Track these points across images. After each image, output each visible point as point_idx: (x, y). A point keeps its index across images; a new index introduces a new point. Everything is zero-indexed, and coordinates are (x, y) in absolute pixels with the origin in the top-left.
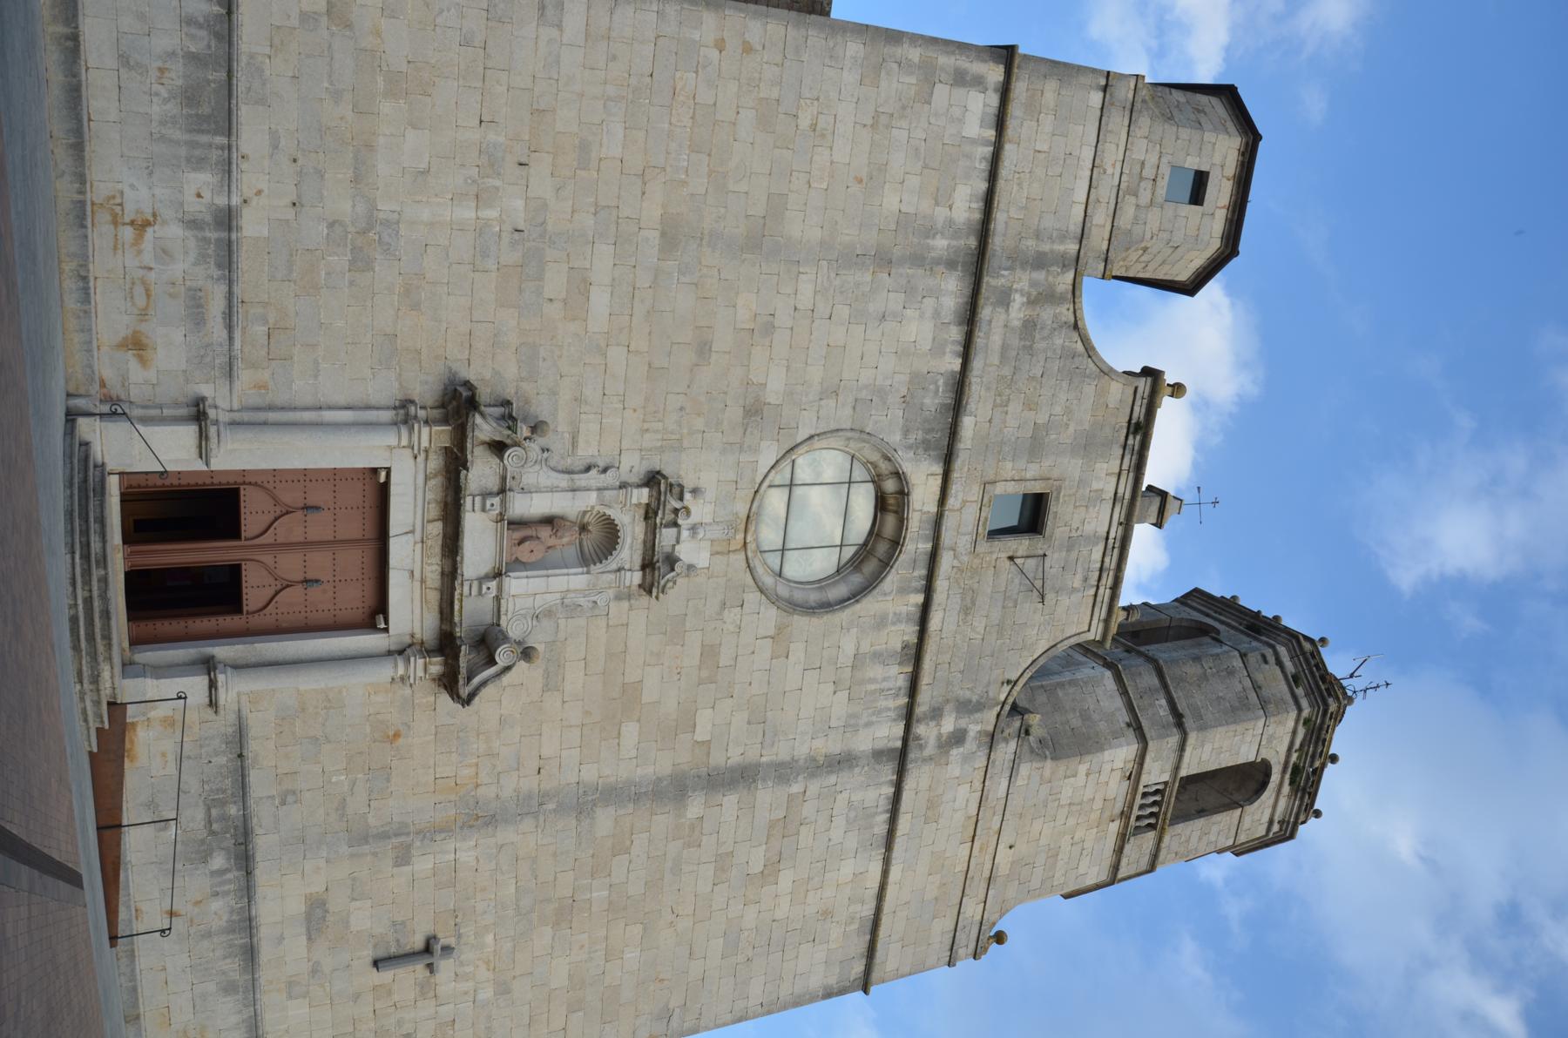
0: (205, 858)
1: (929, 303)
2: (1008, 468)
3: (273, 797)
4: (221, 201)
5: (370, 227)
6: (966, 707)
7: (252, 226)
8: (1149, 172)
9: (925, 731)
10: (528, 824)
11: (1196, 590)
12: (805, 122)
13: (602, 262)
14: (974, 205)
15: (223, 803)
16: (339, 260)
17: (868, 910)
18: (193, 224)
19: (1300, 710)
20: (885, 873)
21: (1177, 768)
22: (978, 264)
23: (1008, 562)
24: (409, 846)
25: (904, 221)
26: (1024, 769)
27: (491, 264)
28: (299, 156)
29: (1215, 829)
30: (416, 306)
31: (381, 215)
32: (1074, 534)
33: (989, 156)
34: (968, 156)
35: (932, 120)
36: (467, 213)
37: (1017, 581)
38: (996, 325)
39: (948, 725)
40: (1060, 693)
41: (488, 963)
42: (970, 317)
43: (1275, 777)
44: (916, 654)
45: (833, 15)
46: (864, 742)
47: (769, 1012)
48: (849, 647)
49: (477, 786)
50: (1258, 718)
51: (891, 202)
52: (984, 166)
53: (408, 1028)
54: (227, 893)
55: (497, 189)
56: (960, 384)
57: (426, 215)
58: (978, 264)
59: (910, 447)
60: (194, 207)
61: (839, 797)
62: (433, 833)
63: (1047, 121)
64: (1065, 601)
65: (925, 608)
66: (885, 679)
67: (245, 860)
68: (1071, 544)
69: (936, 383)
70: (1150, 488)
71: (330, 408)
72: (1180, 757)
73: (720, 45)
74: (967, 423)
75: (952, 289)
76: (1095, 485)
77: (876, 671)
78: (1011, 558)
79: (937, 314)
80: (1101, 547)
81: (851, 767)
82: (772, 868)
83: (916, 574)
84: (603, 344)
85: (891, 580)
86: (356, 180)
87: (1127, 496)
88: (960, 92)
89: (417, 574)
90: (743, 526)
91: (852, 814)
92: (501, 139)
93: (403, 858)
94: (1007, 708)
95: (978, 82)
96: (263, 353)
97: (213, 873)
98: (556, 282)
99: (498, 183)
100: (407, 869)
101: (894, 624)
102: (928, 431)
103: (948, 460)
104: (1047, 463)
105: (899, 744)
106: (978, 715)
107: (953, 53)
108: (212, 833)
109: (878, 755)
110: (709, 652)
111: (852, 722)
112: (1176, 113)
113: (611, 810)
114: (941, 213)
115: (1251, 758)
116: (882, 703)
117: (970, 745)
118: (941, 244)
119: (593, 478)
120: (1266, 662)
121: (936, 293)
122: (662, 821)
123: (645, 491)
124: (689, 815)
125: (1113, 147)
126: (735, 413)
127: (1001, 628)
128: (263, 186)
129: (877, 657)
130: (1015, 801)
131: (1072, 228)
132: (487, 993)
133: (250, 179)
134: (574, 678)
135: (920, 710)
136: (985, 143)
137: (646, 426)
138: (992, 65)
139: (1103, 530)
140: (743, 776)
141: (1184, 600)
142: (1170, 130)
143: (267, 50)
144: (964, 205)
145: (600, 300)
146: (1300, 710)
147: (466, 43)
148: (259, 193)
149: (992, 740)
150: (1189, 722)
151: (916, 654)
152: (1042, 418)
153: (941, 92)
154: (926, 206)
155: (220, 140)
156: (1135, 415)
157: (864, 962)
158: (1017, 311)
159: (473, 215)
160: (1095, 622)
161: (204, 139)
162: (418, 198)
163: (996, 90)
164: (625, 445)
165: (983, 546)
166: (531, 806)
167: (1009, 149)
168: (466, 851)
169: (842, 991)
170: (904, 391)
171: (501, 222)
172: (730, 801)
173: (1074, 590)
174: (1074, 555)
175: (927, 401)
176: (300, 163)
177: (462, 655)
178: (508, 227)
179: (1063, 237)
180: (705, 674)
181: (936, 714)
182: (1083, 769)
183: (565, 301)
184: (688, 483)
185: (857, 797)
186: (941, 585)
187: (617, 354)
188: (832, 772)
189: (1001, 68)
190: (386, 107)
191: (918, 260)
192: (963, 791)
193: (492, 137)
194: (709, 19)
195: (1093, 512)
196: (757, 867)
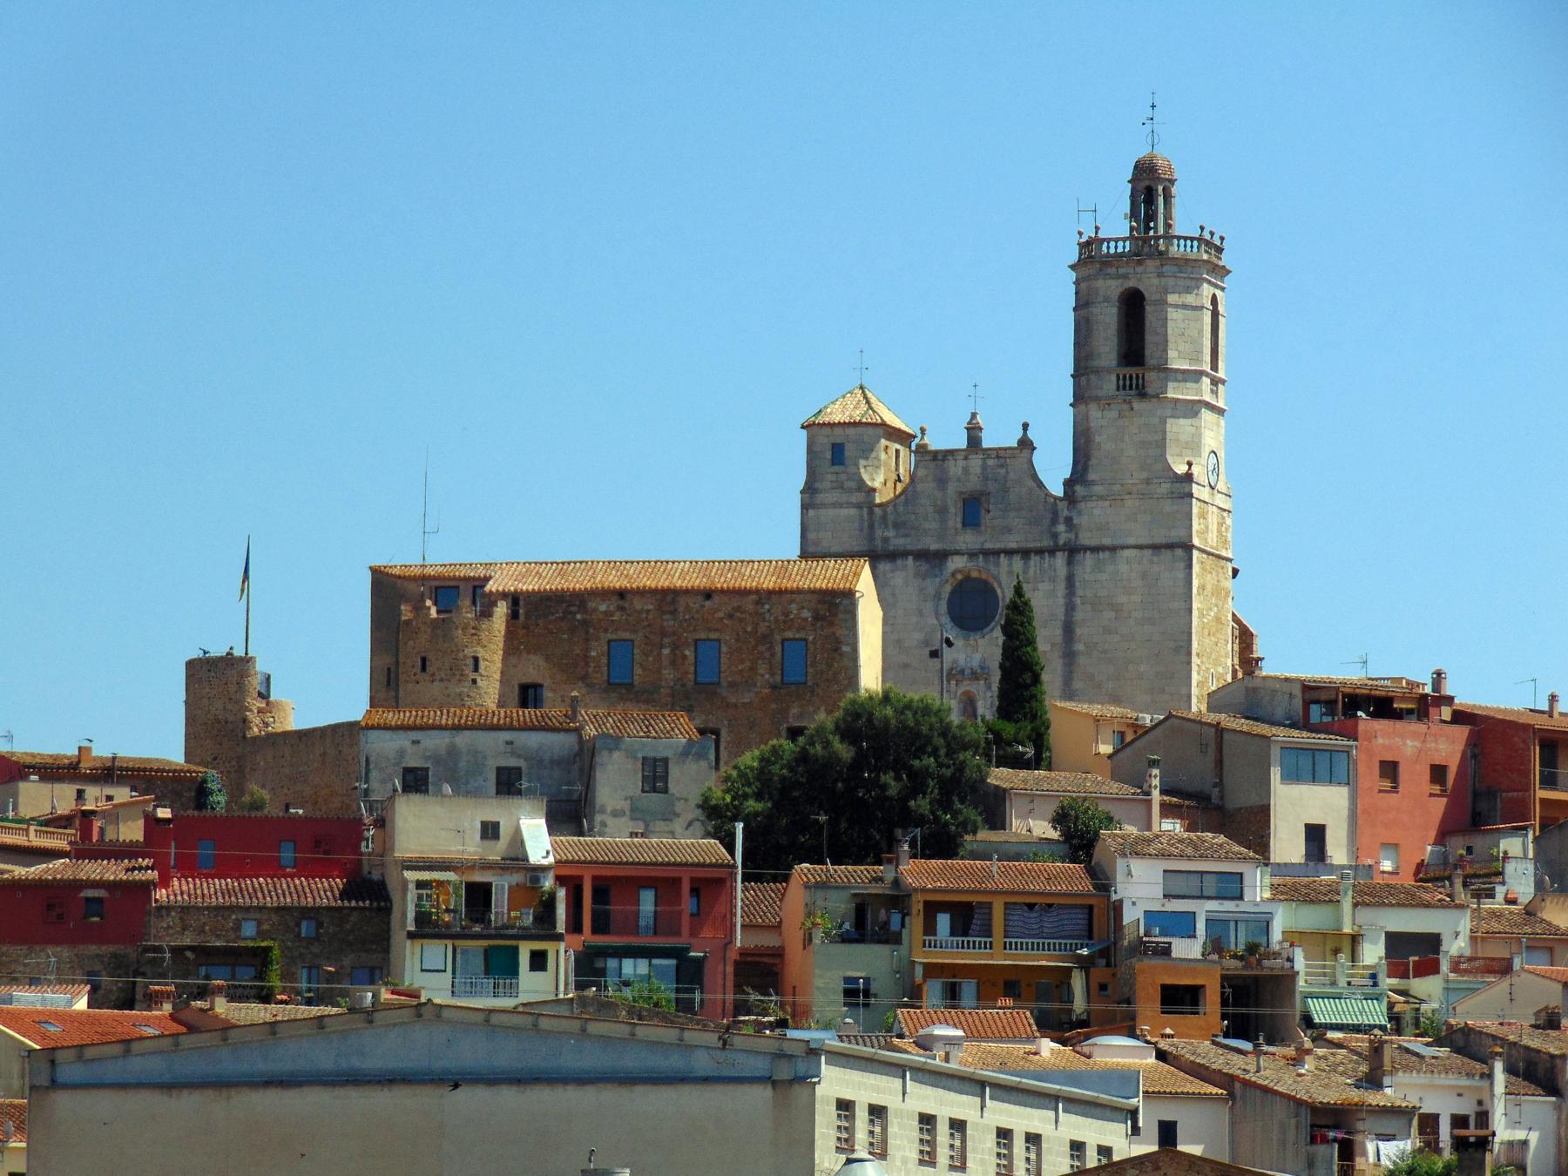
2: (950, 523)
17: (1148, 553)
38: (898, 542)
39: (1061, 528)
45: (1174, 955)
82: (1116, 608)
151: (1026, 553)
152: (931, 509)
158: (890, 533)
167: (834, 549)
185: (1088, 570)
196: (1113, 614)
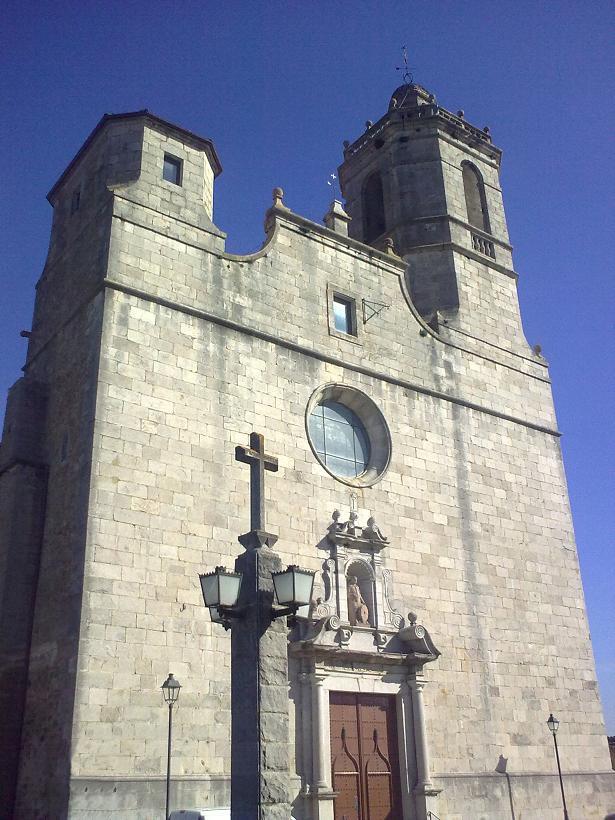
0: (495, 797)
1: (243, 359)
4: (209, 785)
6: (434, 361)
9: (446, 385)
10: (482, 622)
12: (153, 429)
17: (524, 429)
25: (202, 371)
26: (464, 326)
39: (442, 372)
44: (410, 388)
46: (449, 424)
51: (191, 378)
62: (486, 675)
63: (144, 264)
65: (389, 381)
73: (116, 480)
74: (302, 342)
75: (236, 344)
77: (417, 413)
93: (495, 691)
95: (125, 309)
99: (193, 622)
104: (319, 293)
106: (438, 352)
109: (455, 417)
110: (409, 513)
116: (432, 412)
117: (451, 359)
118: (212, 348)
121: (237, 354)
122: (483, 546)
126: (299, 488)
135: (430, 385)
140: (463, 496)
144: (191, 329)
153: (133, 336)
154: (193, 355)
158: (244, 301)
165: (360, 339)
166: (474, 617)
172: (475, 507)
174: (363, 280)
179: (204, 263)
181: (437, 378)
186: (378, 369)
191: (221, 365)
193: (171, 625)
196: (501, 493)
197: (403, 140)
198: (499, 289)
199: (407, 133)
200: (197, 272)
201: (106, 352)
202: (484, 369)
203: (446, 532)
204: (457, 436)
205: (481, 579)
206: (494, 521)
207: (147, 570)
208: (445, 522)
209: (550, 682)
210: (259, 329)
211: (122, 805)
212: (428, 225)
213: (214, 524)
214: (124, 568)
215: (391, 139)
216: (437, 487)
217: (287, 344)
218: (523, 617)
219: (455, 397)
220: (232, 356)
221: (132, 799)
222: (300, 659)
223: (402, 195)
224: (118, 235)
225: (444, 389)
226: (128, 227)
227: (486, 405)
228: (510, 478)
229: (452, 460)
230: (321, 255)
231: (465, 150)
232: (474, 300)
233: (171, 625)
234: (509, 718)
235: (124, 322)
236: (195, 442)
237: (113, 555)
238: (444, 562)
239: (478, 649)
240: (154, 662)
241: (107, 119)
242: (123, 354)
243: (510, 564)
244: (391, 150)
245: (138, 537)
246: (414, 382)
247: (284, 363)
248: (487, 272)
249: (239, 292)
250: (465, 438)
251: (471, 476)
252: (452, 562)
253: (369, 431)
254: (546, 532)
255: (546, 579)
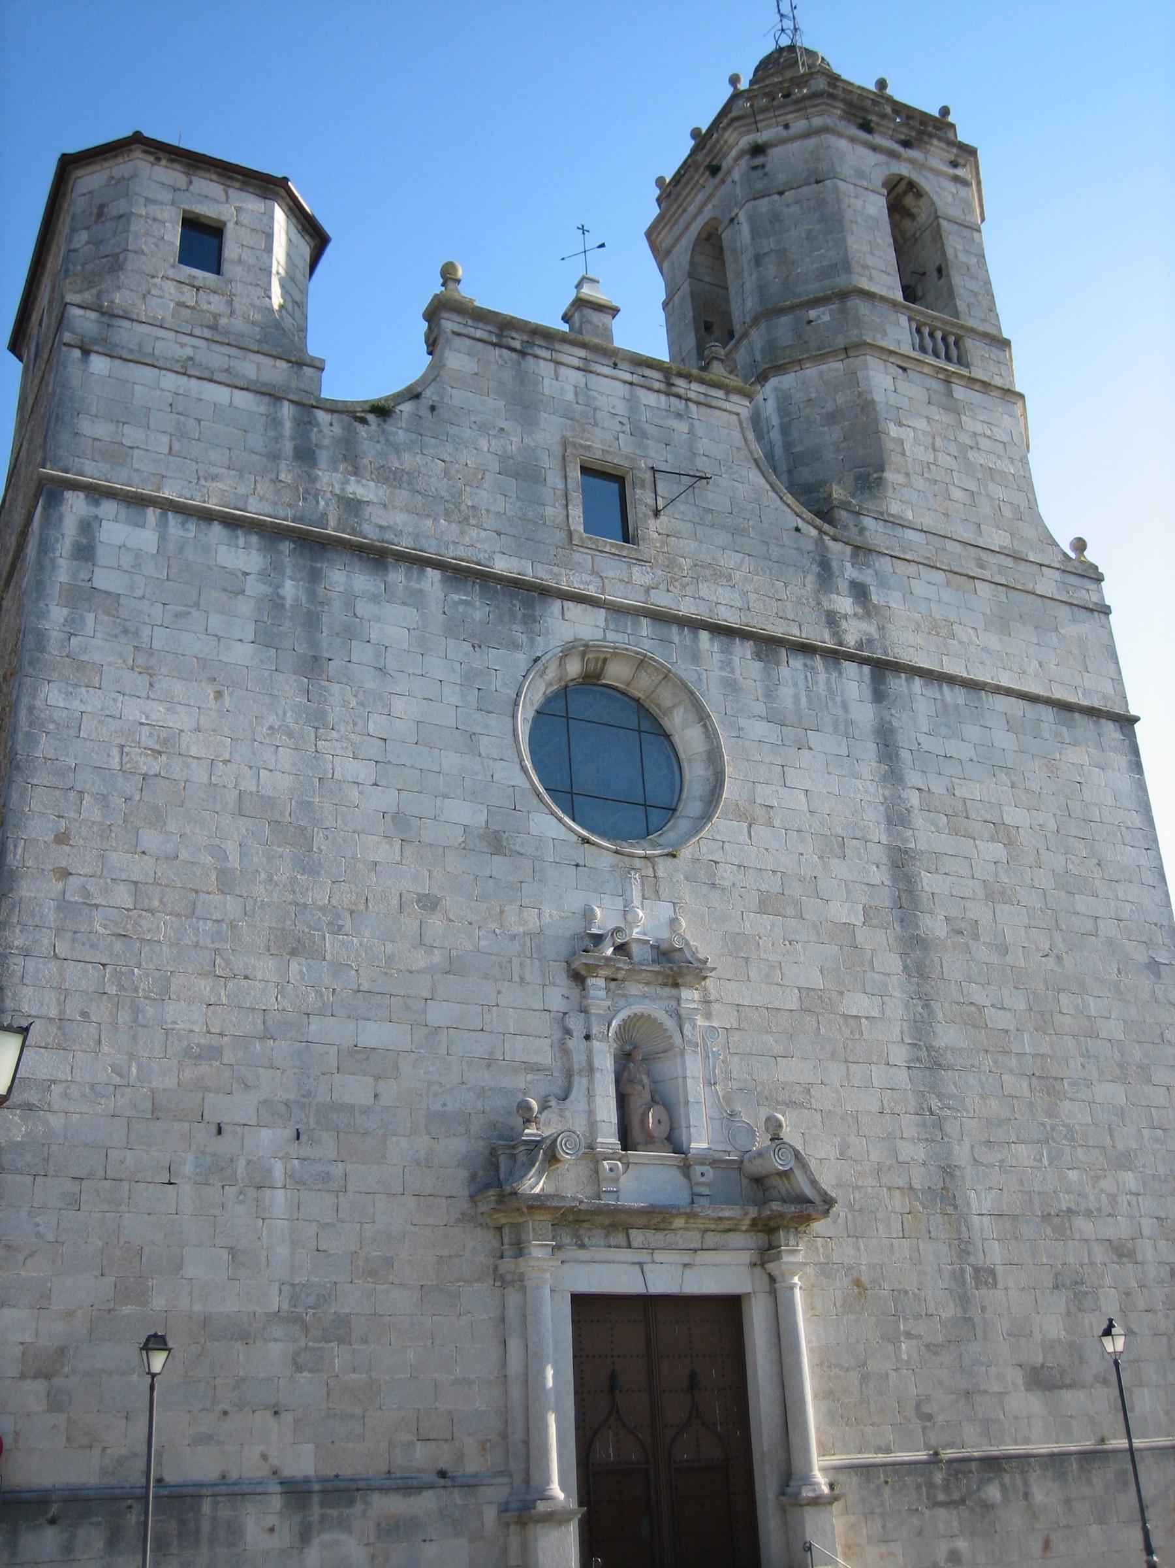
0: (988, 1506)
1: (363, 608)
2: (553, 512)
3: (924, 1429)
4: (277, 1502)
5: (299, 1320)
6: (826, 573)
7: (303, 1463)
8: (189, 297)
9: (853, 632)
10: (952, 1128)
11: (649, 234)
12: (154, 766)
13: (331, 1032)
14: (241, 541)
15: (931, 1485)
16: (339, 1357)
17: (1047, 714)
18: (305, 1536)
19: (825, 130)
20: (1009, 692)
21: (894, 304)
22: (314, 545)
23: (663, 518)
24: (977, 1270)
25: (265, 638)
26: (895, 508)
27: (337, 1170)
28: (219, 1408)
29: (963, 257)
30: (389, 1262)
31: (285, 1306)
32: (627, 429)
33: (180, 518)
34: (181, 549)
35: (140, 593)
36: (279, 1199)
37: (682, 508)
39: (844, 604)
40: (798, 449)
41: (1097, 1178)
42: (376, 556)
43: (905, 170)
44: (768, 645)
46: (864, 713)
47: (1156, 840)
48: (759, 729)
49: (911, 1188)
50: (836, 189)
51: (242, 653)
52: (192, 527)
53: (1164, 1272)
54: (1026, 1483)
55: (249, 1162)
56: (460, 575)
57: (282, 1251)
58: (314, 545)
59: (532, 641)
60: (284, 1538)
61: (924, 747)
62: (963, 1247)
63: (132, 434)
64: (704, 445)
65: (720, 631)
66: (795, 684)
67: (992, 1465)
68: (638, 433)
69: (456, 604)
70: (566, 318)
71: (504, 1364)
72: (882, 299)
73: (65, 874)
74: (502, 566)
75: (342, 577)
76: (570, 396)
77: (786, 694)
78: (657, 513)
79: (375, 598)
80: (642, 393)
81: (892, 731)
82: (1002, 832)
83: (676, 639)
84: (425, 1031)
85: (684, 670)
86: (244, 1336)
87: (582, 353)
88: (102, 553)
89: (686, 1258)
90: (626, 859)
91: (944, 731)
92: (190, 1157)
93: (986, 1276)
94: (826, 527)
95: (87, 527)
96: (445, 1446)
97: (1005, 1498)
98: (355, 1090)
99: (242, 1162)
100: (1000, 1270)
101: (733, 671)
102: (513, 616)
103: (545, 593)
104: (546, 462)
105: (866, 669)
106: (835, 565)
107: (53, 560)
108: (962, 1501)
109: (879, 696)
110: (765, 904)
111: (842, 727)
112: (107, 249)
113: (939, 1029)
114: (254, 587)
115: (882, 202)
116: (821, 688)
117: (867, 577)
118: (290, 590)
119: (575, 1044)
120: (763, 166)
121: (350, 600)
122: (951, 965)
123: (590, 981)
124: (943, 934)
125: (159, 345)
126: (499, 866)
127: (736, 532)
128: (257, 1451)
129: (770, 693)
130: (928, 522)
131: (262, 409)
132: (1129, 1180)
133: (248, 1465)
134: (794, 1071)
135: (823, 637)
136: (163, 522)
137: (516, 978)
138: (65, 508)
139: (623, 390)
140: (901, 863)
141: (660, 254)
142: (133, 263)
143: (96, 1451)
144: (242, 557)
145: (375, 1034)
146: (825, 130)
147: (76, 1203)
148: (264, 1457)
149: (862, 552)
150: (841, 282)
152: (494, 465)
153: (104, 580)
154: (245, 607)
155: (206, 1507)
156: (485, 336)
157: (1103, 721)
158: (364, 490)
159: (281, 1192)
160: (728, 406)
161: (206, 1527)
162: (263, 1259)
163: (97, 503)
164: (538, 1005)
165: (646, 551)
166: (934, 1125)
168: (980, 1201)
169: (1135, 750)
170: (467, 646)
171: (286, 1158)
172: (928, 882)
173: (691, 431)
174: (651, 430)
175: (478, 615)
176: (227, 1407)
177: (771, 1203)
178: (294, 1149)
179: (274, 422)
180: (790, 911)
181: (832, 620)
182: (894, 431)
183: (377, 1078)
184: (577, 926)
185: (924, 725)
186: (687, 608)
187: (436, 1014)
188: (897, 754)
189: (68, 494)
190: (158, 1302)
191: (312, 622)
192: (918, 587)
193: (188, 1169)
194: (26, 890)
195: (602, 402)
196: (997, 851)
197: (758, 150)
198: (979, 428)
199: (764, 136)
200: (257, 440)
201: (43, 615)
202: (947, 594)
203: (859, 939)
204: (886, 739)
205: (947, 1036)
206: (980, 912)
207: (132, 1056)
208: (858, 920)
209: (1122, 1252)
210: (404, 544)
211: (68, 1549)
212: (812, 314)
213: (294, 953)
214: (79, 1054)
215: (734, 153)
216: (836, 846)
217: (468, 570)
218: (1051, 1112)
219: (879, 655)
220: (337, 604)
221: (92, 1537)
222: (499, 1229)
223: (758, 260)
224: (76, 382)
225: (851, 640)
226: (98, 364)
227: (952, 667)
228: (1014, 816)
229: (871, 787)
230: (549, 386)
231: (892, 154)
232: (917, 452)
233: (188, 1169)
234: (1020, 1332)
235: (85, 552)
236: (250, 785)
237: (53, 1030)
238: (858, 1004)
239: (945, 1193)
240: (146, 1250)
241: (69, 165)
242: (83, 620)
243: (1018, 1002)
244: (736, 175)
245: (113, 990)
246: (777, 629)
247: (461, 609)
248: (950, 394)
249: (355, 473)
250: (904, 740)
251: (919, 820)
252: (879, 1007)
253: (676, 739)
254: (1107, 928)
255: (1112, 1028)
